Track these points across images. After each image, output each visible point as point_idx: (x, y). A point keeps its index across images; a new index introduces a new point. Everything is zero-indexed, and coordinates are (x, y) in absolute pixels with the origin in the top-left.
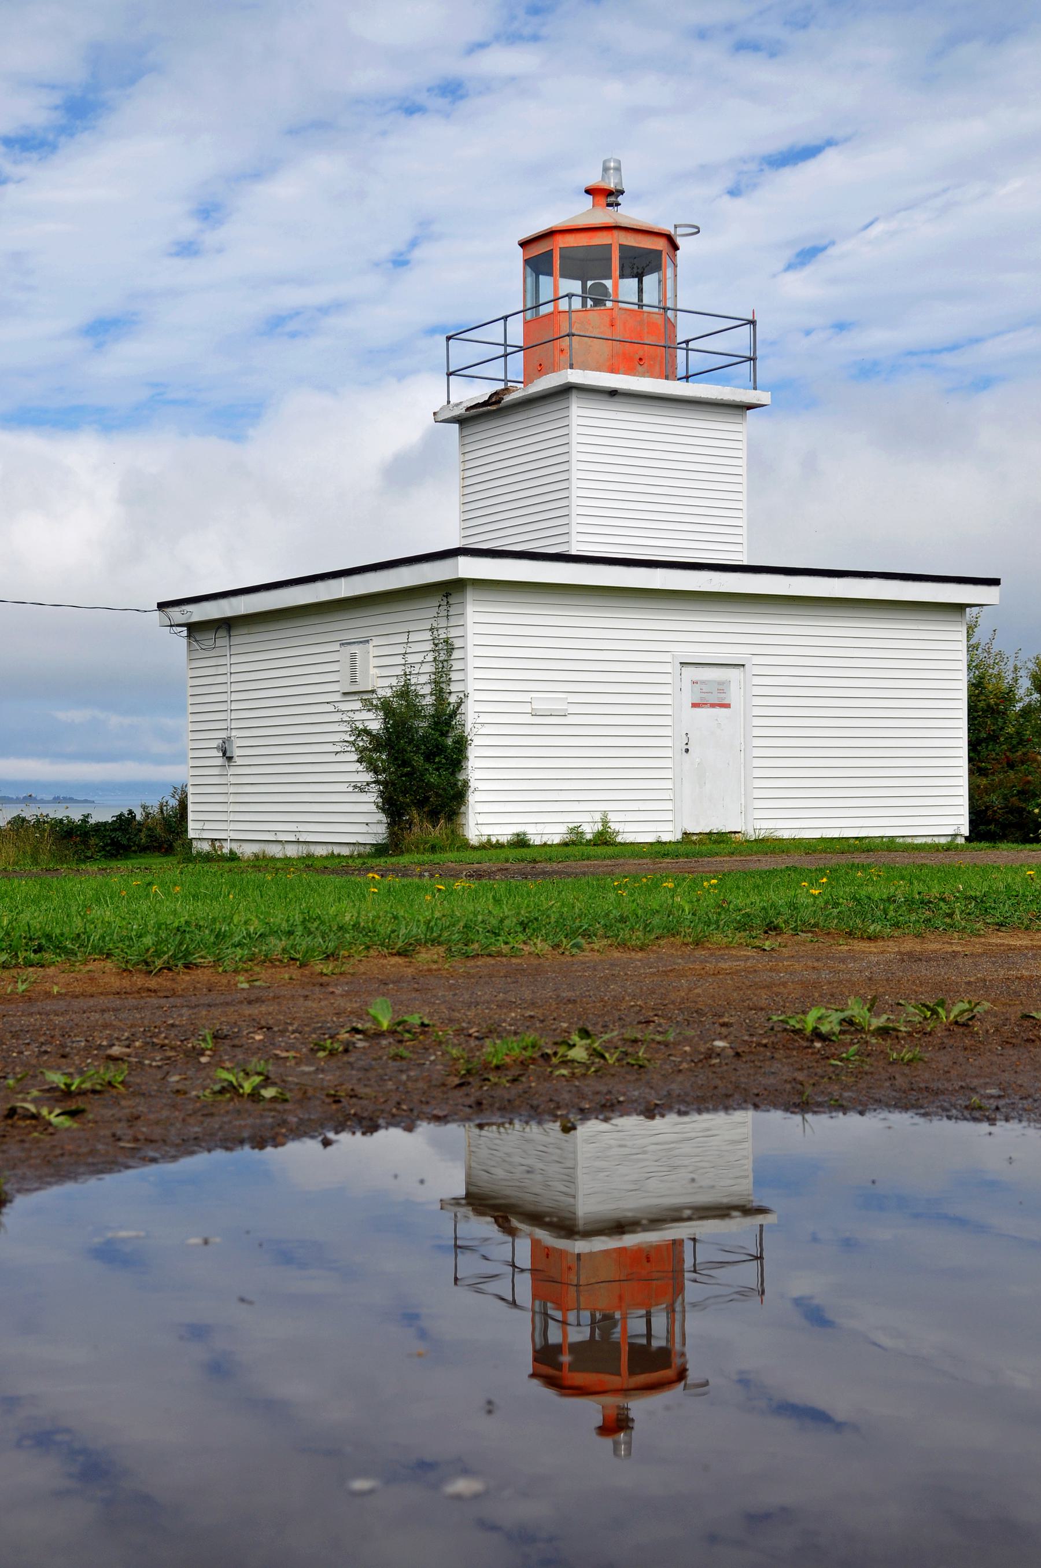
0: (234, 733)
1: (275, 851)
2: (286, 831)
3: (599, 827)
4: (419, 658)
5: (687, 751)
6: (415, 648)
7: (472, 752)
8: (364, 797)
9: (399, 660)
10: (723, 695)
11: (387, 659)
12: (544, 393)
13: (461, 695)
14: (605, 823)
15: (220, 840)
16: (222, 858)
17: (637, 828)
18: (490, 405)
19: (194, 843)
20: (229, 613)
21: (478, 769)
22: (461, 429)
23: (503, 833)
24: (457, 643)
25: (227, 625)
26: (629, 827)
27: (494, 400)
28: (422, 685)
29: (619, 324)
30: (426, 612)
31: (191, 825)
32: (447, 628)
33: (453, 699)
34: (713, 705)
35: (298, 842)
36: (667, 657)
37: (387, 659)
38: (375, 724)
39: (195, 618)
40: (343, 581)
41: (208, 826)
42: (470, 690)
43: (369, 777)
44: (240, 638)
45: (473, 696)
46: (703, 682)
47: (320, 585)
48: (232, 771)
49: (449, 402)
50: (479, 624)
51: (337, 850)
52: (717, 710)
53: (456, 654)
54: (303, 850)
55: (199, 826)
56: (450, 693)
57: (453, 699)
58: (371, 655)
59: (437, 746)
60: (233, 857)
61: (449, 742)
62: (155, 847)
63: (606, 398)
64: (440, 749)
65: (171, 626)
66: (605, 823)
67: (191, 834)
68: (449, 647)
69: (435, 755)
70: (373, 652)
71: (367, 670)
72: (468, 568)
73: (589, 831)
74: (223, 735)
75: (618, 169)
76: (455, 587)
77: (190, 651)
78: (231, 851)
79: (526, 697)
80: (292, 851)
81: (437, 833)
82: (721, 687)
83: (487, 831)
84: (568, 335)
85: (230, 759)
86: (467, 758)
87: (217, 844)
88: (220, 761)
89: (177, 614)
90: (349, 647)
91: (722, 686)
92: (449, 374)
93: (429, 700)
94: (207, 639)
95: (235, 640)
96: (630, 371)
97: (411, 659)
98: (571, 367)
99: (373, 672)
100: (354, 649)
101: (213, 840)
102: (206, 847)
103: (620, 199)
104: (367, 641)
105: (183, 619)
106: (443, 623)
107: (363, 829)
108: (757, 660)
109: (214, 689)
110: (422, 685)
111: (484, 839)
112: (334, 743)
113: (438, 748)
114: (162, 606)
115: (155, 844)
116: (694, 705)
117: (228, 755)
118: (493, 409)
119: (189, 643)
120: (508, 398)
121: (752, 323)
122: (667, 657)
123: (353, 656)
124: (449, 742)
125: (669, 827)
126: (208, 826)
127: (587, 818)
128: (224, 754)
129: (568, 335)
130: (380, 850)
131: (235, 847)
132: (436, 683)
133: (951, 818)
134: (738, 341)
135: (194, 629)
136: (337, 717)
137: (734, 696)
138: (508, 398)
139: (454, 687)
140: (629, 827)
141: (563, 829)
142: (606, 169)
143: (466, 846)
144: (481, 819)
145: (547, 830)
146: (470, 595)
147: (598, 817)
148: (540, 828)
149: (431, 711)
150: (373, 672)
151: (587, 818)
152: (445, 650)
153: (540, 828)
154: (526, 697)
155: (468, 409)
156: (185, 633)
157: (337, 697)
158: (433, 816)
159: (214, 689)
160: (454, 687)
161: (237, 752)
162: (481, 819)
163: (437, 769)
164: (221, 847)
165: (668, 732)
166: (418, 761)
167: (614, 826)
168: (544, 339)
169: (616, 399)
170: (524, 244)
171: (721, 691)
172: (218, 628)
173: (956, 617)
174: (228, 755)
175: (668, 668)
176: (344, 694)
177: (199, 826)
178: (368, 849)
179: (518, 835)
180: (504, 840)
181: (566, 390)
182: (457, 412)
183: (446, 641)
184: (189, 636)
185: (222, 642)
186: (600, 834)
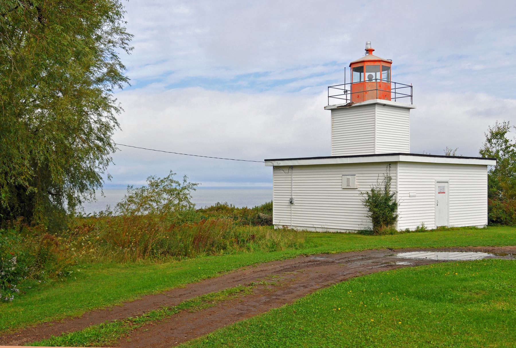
1: (309, 230)
3: (421, 226)
6: (380, 178)
7: (399, 207)
14: (422, 225)
17: (430, 226)
21: (400, 211)
22: (332, 114)
23: (404, 229)
24: (393, 178)
29: (382, 87)
31: (274, 221)
33: (391, 193)
37: (369, 182)
41: (281, 221)
44: (295, 172)
45: (399, 192)
50: (401, 171)
53: (392, 181)
57: (391, 193)
68: (390, 179)
72: (402, 158)
75: (370, 44)
76: (396, 163)
79: (408, 192)
81: (388, 229)
83: (402, 228)
86: (397, 209)
88: (289, 204)
95: (294, 171)
96: (384, 99)
100: (348, 177)
103: (132, 38)
107: (358, 226)
108: (451, 181)
114: (265, 160)
121: (412, 87)
123: (348, 179)
126: (281, 221)
133: (482, 220)
134: (408, 91)
135: (275, 168)
138: (353, 105)
139: (391, 189)
141: (416, 227)
142: (367, 44)
145: (413, 228)
146: (399, 165)
152: (389, 179)
154: (408, 192)
160: (391, 189)
166: (382, 209)
167: (426, 226)
171: (444, 189)
178: (356, 232)
180: (404, 230)
181: (374, 104)
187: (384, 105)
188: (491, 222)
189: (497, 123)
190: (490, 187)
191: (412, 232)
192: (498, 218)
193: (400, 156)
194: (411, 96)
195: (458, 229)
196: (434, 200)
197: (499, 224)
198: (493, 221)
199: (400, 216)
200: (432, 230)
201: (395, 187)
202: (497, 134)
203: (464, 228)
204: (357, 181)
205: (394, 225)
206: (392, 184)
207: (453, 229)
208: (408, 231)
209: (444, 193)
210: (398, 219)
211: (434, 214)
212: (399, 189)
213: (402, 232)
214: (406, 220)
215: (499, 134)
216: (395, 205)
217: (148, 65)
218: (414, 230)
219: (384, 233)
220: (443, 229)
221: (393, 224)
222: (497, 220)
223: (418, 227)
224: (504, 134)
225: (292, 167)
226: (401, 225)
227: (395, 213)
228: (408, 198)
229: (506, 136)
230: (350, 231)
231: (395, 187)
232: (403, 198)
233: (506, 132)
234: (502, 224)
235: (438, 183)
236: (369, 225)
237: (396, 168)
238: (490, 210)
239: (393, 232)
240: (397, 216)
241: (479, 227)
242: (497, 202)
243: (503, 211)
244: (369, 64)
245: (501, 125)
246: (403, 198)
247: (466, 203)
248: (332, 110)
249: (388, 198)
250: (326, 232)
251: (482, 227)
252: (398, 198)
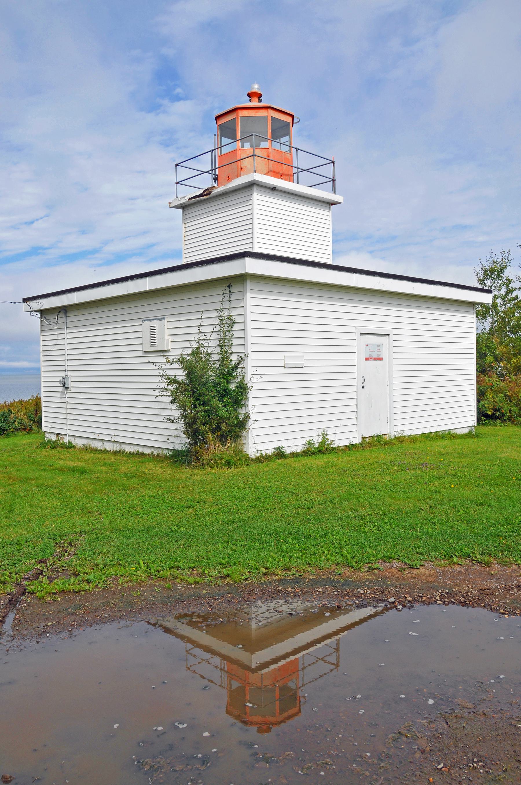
0: (69, 373)
1: (98, 445)
2: (105, 434)
3: (320, 439)
4: (210, 329)
5: (363, 387)
6: (207, 322)
7: (251, 395)
8: (173, 426)
9: (196, 330)
10: (379, 353)
11: (182, 332)
12: (237, 188)
13: (243, 355)
14: (324, 435)
15: (62, 434)
16: (63, 446)
18: (203, 196)
19: (46, 435)
20: (67, 303)
21: (255, 405)
22: (183, 211)
23: (269, 449)
24: (238, 319)
25: (64, 310)
26: (337, 437)
27: (206, 193)
28: (211, 346)
30: (215, 298)
32: (229, 308)
33: (234, 357)
34: (375, 359)
35: (114, 441)
36: (353, 330)
37: (182, 332)
38: (181, 374)
39: (45, 307)
40: (147, 279)
41: (54, 425)
42: (249, 352)
43: (177, 413)
44: (72, 318)
45: (252, 355)
46: (371, 345)
47: (130, 283)
48: (68, 395)
49: (177, 197)
50: (255, 304)
51: (141, 450)
52: (377, 362)
53: (236, 327)
54: (117, 447)
55: (49, 425)
56: (232, 353)
57: (234, 357)
58: (166, 327)
59: (225, 390)
60: (70, 446)
61: (232, 387)
62: (23, 429)
63: (270, 191)
64: (227, 392)
65: (31, 311)
66: (324, 435)
67: (44, 429)
69: (224, 396)
70: (167, 325)
71: (163, 338)
72: (252, 266)
73: (317, 440)
74: (63, 374)
76: (242, 278)
77: (42, 325)
78: (69, 442)
79: (280, 356)
80: (109, 447)
81: (226, 450)
82: (378, 348)
83: (260, 447)
84: (253, 156)
85: (67, 388)
86: (247, 399)
87: (60, 436)
88: (61, 389)
89: (35, 305)
90: (149, 322)
91: (379, 347)
92: (177, 183)
93: (215, 357)
94: (53, 318)
95: (69, 319)
97: (203, 329)
98: (255, 171)
99: (167, 338)
100: (153, 323)
101: (57, 434)
102: (53, 438)
104: (164, 319)
105: (38, 308)
106: (226, 305)
109: (302, 420)
110: (211, 346)
111: (258, 454)
112: (154, 390)
113: (226, 392)
114: (25, 300)
115: (23, 427)
116: (367, 359)
117: (66, 386)
118: (206, 198)
119: (41, 321)
120: (215, 192)
121: (333, 163)
122: (353, 330)
123: (153, 328)
124: (232, 387)
125: (355, 435)
126: (54, 425)
127: (314, 433)
128: (64, 385)
129: (253, 156)
130: (178, 458)
131: (71, 439)
132: (222, 347)
133: (463, 416)
135: (43, 313)
136: (157, 373)
137: (385, 354)
138: (215, 192)
139: (234, 349)
140: (337, 437)
141: (304, 442)
143: (248, 461)
144: (257, 440)
145: (295, 445)
146: (249, 285)
147: (320, 432)
148: (290, 443)
149: (217, 365)
150: (167, 338)
151: (314, 433)
153: (290, 443)
154: (280, 356)
155: (190, 199)
156: (39, 316)
157: (140, 354)
158: (223, 438)
159: (302, 420)
160: (234, 349)
161: (71, 385)
162: (257, 440)
163: (225, 406)
164: (63, 439)
165: (354, 376)
166: (211, 400)
168: (228, 165)
169: (275, 192)
170: (217, 118)
171: (379, 350)
172: (59, 312)
173: (471, 309)
174: (66, 386)
175: (353, 336)
176: (145, 352)
177: (49, 425)
179: (278, 448)
180: (270, 452)
181: (251, 185)
182: (183, 201)
183: (229, 318)
184: (41, 317)
185: (62, 320)
186: (322, 443)
187: (274, 189)
188: (483, 418)
189: (491, 253)
190: (480, 355)
191: (294, 455)
192: (496, 410)
193: (248, 260)
194: (334, 180)
195: (413, 439)
196: (354, 376)
197: (498, 421)
198: (487, 416)
199: (253, 417)
200: (350, 447)
201: (241, 342)
202: (492, 271)
203: (427, 437)
204: (168, 332)
205: (243, 440)
206: (236, 334)
207: (400, 440)
208: (280, 454)
209: (380, 359)
210: (250, 424)
211: (354, 408)
212: (250, 349)
213: (262, 459)
214: (271, 426)
215: (495, 271)
216: (243, 388)
217: (127, 237)
218: (299, 450)
219: (213, 463)
220: (378, 442)
221: (239, 437)
222: (493, 414)
223: (309, 443)
224: (502, 271)
225: (64, 310)
226: (259, 440)
227: (243, 411)
228: (283, 370)
229: (506, 273)
230: (160, 451)
231: (241, 342)
232: (261, 371)
233: (505, 268)
234: (504, 421)
235: (365, 337)
236: (182, 443)
237: (244, 292)
238: (481, 395)
239: (240, 459)
240: (247, 417)
241: (459, 432)
242: (494, 380)
243: (505, 395)
244: (246, 113)
245: (499, 257)
246: (261, 371)
247: (423, 382)
248: (183, 207)
249: (227, 372)
250: (119, 452)
251: (466, 431)
252: (250, 371)
